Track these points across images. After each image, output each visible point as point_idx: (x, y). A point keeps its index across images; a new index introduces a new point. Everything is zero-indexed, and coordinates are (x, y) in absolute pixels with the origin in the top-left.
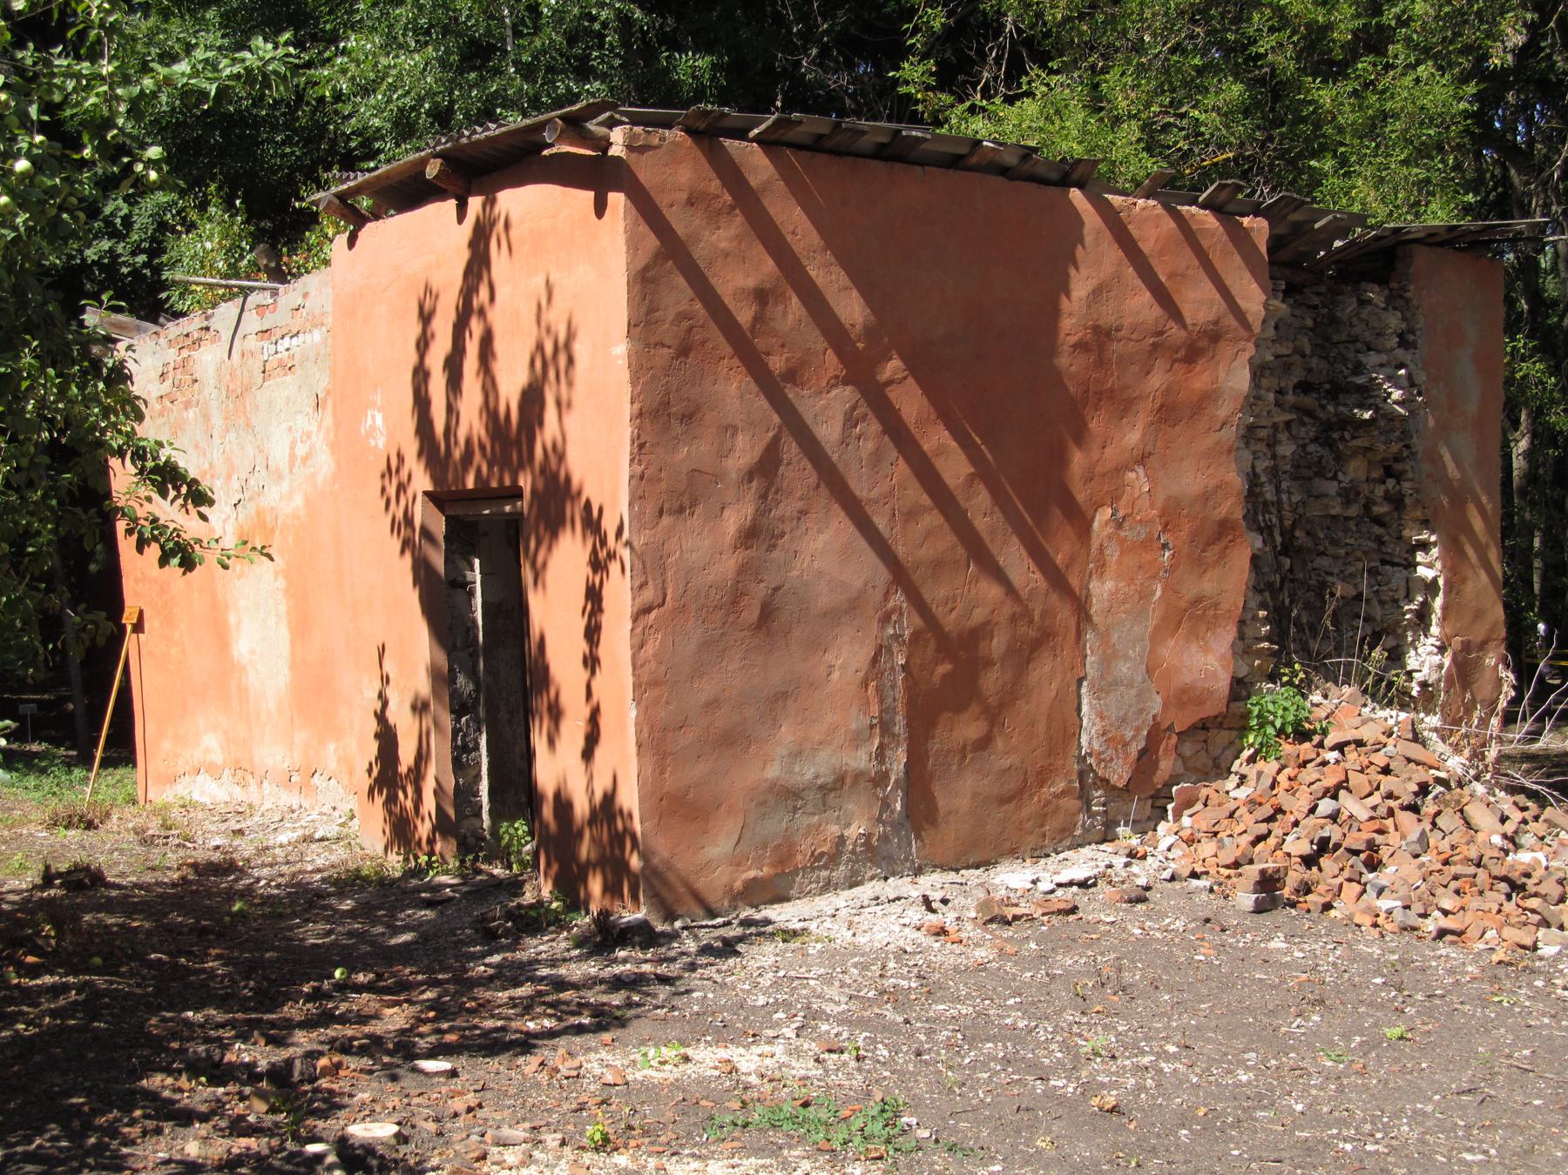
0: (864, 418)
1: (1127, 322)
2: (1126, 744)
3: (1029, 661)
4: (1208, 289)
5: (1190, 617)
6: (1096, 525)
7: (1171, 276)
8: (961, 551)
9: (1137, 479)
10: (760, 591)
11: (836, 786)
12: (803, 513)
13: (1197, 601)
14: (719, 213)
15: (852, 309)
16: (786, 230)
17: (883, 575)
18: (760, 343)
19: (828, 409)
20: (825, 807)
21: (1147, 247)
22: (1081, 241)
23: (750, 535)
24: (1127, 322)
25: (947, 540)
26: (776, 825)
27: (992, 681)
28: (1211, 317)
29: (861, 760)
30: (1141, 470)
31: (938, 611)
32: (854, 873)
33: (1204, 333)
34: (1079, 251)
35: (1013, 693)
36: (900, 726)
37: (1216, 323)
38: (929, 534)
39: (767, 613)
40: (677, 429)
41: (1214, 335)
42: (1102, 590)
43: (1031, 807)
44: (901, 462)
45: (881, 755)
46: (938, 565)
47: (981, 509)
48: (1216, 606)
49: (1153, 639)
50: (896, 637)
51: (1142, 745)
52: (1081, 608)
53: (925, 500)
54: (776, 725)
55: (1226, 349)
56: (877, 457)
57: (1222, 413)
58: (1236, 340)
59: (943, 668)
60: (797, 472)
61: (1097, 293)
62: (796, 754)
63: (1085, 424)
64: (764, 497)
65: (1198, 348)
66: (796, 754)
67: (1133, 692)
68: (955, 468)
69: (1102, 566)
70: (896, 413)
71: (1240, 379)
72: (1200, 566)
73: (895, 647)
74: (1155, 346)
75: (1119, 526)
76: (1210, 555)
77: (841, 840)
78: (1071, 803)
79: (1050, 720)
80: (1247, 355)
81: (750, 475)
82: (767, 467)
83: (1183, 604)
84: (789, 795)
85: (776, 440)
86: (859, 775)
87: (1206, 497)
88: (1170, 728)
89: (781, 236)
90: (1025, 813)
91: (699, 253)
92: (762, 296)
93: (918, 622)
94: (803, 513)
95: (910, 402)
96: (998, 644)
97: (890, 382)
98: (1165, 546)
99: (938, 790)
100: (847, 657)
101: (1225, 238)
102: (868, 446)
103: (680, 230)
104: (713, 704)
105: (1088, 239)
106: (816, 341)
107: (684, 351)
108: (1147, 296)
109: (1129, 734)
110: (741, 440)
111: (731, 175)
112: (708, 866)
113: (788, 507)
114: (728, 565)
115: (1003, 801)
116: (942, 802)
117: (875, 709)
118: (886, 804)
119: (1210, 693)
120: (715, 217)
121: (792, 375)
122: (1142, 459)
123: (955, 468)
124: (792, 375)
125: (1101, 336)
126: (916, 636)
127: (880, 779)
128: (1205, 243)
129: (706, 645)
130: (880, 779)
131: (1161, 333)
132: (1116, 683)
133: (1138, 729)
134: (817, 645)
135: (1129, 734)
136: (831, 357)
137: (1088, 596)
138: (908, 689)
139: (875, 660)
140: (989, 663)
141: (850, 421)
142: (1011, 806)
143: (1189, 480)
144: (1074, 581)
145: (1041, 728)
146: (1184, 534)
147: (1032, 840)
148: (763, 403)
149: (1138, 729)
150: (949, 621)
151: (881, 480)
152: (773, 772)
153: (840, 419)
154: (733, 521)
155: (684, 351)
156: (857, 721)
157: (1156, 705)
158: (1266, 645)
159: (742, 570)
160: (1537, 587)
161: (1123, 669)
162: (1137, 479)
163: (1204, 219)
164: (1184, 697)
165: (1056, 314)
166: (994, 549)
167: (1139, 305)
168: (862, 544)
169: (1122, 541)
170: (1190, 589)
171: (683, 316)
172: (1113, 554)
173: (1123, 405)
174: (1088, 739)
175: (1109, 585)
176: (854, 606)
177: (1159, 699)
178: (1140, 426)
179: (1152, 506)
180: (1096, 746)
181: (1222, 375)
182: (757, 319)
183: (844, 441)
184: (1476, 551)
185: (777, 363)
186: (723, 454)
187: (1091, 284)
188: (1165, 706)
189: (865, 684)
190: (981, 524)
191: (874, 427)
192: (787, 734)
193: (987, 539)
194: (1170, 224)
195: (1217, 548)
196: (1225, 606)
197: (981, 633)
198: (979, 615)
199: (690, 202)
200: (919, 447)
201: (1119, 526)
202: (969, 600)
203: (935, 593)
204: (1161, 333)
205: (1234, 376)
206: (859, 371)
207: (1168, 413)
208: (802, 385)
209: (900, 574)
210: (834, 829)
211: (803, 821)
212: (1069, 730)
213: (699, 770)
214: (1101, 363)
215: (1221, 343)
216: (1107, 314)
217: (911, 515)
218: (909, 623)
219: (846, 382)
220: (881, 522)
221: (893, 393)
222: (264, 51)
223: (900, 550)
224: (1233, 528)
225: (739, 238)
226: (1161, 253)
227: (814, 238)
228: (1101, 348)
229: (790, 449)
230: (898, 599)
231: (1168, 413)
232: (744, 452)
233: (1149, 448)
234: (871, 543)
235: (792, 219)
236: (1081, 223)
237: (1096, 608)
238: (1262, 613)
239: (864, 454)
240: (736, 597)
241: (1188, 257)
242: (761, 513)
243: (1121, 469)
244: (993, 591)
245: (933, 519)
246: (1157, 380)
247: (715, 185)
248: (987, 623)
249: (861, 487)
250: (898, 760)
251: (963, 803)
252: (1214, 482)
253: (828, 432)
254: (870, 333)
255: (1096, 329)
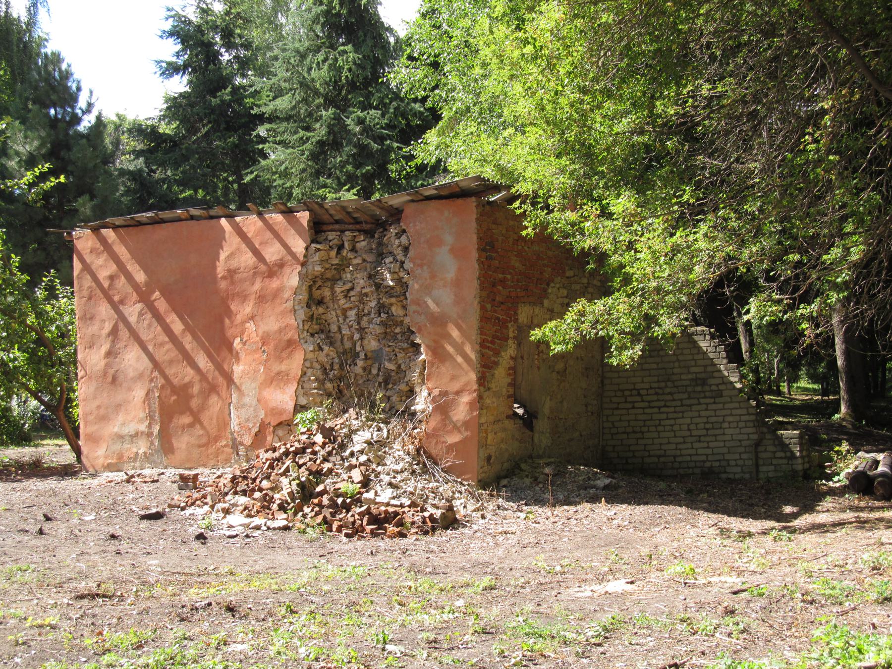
0: (146, 313)
1: (242, 265)
2: (249, 429)
3: (208, 396)
4: (277, 246)
5: (276, 379)
6: (235, 345)
7: (260, 244)
8: (180, 356)
9: (251, 326)
10: (111, 372)
11: (136, 435)
12: (126, 346)
13: (279, 373)
14: (100, 253)
15: (140, 277)
16: (120, 255)
17: (150, 366)
18: (111, 293)
19: (133, 311)
20: (132, 442)
21: (250, 235)
22: (224, 238)
23: (109, 354)
24: (242, 265)
25: (175, 353)
26: (117, 447)
27: (195, 403)
28: (279, 257)
29: (143, 427)
30: (252, 322)
31: (172, 378)
32: (142, 465)
33: (275, 265)
34: (224, 242)
35: (203, 407)
36: (157, 416)
37: (281, 260)
38: (168, 351)
39: (114, 379)
40: (89, 322)
41: (281, 265)
42: (238, 370)
43: (212, 450)
44: (159, 327)
45: (150, 426)
46: (171, 362)
47: (188, 342)
48: (288, 375)
49: (260, 388)
50: (156, 387)
51: (257, 430)
52: (229, 378)
53: (167, 339)
54: (118, 414)
55: (287, 270)
56: (150, 325)
57: (286, 296)
58: (292, 265)
59: (174, 398)
60: (124, 333)
61: (229, 258)
62: (123, 424)
63: (229, 307)
64: (113, 341)
65: (274, 270)
66: (123, 424)
67: (252, 409)
68: (178, 327)
69: (238, 360)
70: (157, 310)
71: (294, 281)
72: (281, 360)
73: (155, 390)
74: (255, 273)
75: (244, 344)
76: (284, 355)
77: (137, 453)
78: (228, 450)
79: (218, 418)
80: (298, 270)
81: (109, 335)
82: (114, 332)
83: (273, 374)
84: (120, 437)
85: (116, 323)
86: (142, 433)
87: (280, 331)
88: (269, 423)
89: (118, 257)
90: (210, 451)
91: (94, 267)
92: (112, 278)
93: (163, 381)
94: (126, 346)
95: (162, 305)
96: (196, 389)
97: (155, 300)
98: (264, 351)
99: (174, 441)
100: (139, 393)
101: (286, 224)
102: (146, 322)
103: (88, 261)
104: (99, 407)
105: (227, 236)
106: (130, 289)
107: (90, 298)
108: (250, 254)
109: (251, 425)
110: (107, 323)
111: (103, 241)
112: (97, 458)
113: (121, 345)
114: (102, 363)
115: (200, 446)
116: (176, 444)
117: (147, 411)
118: (152, 443)
119: (285, 410)
120: (99, 255)
121: (122, 302)
122: (252, 318)
123: (178, 327)
124: (122, 302)
125: (231, 273)
126: (163, 387)
127: (150, 435)
128: (276, 228)
129: (97, 388)
130: (150, 435)
131: (256, 268)
132: (244, 405)
133: (255, 424)
134: (130, 389)
135: (251, 425)
136: (135, 294)
137: (232, 371)
138: (160, 405)
139: (147, 394)
140: (192, 396)
141: (141, 314)
142: (204, 449)
143: (271, 324)
144: (226, 367)
145: (215, 421)
146: (272, 346)
147: (212, 462)
148: (113, 312)
149: (255, 424)
150: (176, 381)
151: (150, 331)
152: (116, 430)
153: (137, 314)
154: (105, 348)
155: (90, 298)
156: (142, 415)
157: (262, 414)
158: (315, 391)
159: (106, 365)
160: (840, 362)
161: (247, 400)
162: (251, 326)
163: (277, 218)
164: (274, 411)
165: (214, 267)
166: (193, 355)
167: (247, 259)
168: (144, 355)
169: (246, 350)
170: (276, 367)
171: (90, 287)
172: (242, 355)
173: (244, 298)
174: (234, 424)
175: (241, 367)
176: (141, 376)
177: (263, 412)
178: (251, 304)
179: (257, 336)
180: (236, 429)
181: (285, 280)
182: (110, 285)
183: (138, 322)
184: (453, 347)
185: (116, 298)
186: (101, 329)
187: (227, 253)
188: (266, 415)
189: (144, 402)
190: (188, 347)
191: (149, 316)
192: (121, 418)
193: (190, 351)
194: (260, 223)
195: (287, 351)
196: (292, 375)
197: (189, 385)
198: (187, 379)
199: (91, 252)
200: (165, 321)
201: (244, 344)
202: (183, 374)
203: (170, 372)
204: (256, 268)
205: (292, 279)
206: (144, 297)
207: (262, 299)
208: (125, 305)
209: (156, 365)
210: (135, 450)
211: (126, 446)
212: (224, 423)
213: (96, 427)
214: (233, 283)
215: (285, 268)
216: (234, 264)
217: (162, 344)
218: (161, 381)
219: (140, 302)
220: (150, 348)
221: (156, 304)
222: (364, 171)
223: (157, 357)
224: (295, 343)
225: (106, 260)
226: (257, 236)
227: (129, 256)
228: (232, 277)
229: (121, 326)
230: (156, 374)
231: (262, 299)
232: (108, 327)
233: (255, 313)
234: (147, 355)
235: (121, 251)
236: (224, 231)
237: (236, 377)
238: (313, 378)
239: (145, 325)
240: (105, 374)
241: (269, 235)
242: (111, 347)
243: (243, 323)
244: (190, 371)
245: (169, 346)
246: (257, 286)
247: (98, 245)
248: (190, 382)
249: (144, 337)
250: (156, 429)
251: (184, 446)
252: (283, 325)
253: (133, 319)
254: (147, 284)
255: (229, 271)
